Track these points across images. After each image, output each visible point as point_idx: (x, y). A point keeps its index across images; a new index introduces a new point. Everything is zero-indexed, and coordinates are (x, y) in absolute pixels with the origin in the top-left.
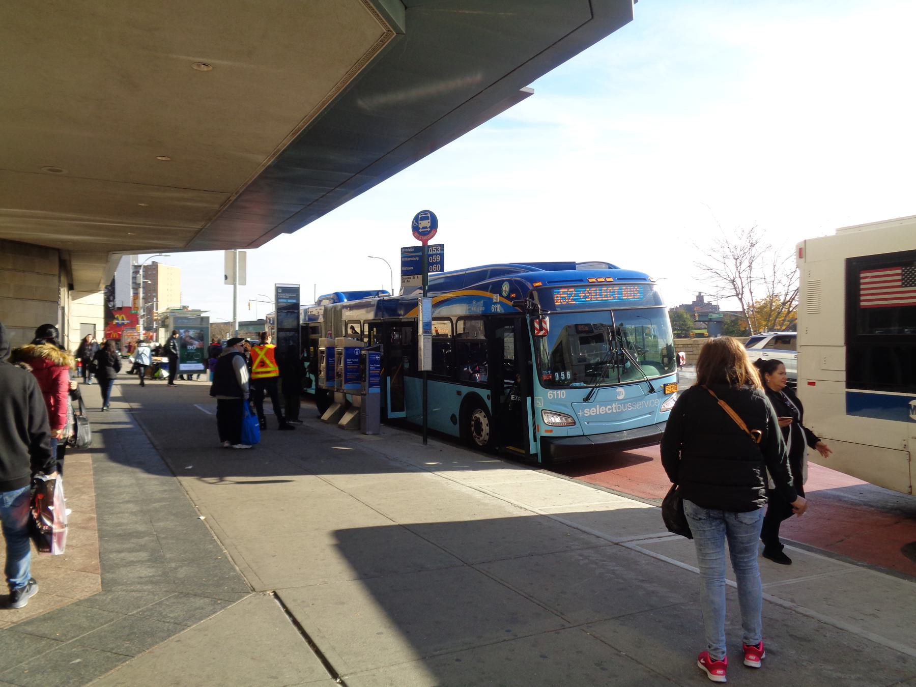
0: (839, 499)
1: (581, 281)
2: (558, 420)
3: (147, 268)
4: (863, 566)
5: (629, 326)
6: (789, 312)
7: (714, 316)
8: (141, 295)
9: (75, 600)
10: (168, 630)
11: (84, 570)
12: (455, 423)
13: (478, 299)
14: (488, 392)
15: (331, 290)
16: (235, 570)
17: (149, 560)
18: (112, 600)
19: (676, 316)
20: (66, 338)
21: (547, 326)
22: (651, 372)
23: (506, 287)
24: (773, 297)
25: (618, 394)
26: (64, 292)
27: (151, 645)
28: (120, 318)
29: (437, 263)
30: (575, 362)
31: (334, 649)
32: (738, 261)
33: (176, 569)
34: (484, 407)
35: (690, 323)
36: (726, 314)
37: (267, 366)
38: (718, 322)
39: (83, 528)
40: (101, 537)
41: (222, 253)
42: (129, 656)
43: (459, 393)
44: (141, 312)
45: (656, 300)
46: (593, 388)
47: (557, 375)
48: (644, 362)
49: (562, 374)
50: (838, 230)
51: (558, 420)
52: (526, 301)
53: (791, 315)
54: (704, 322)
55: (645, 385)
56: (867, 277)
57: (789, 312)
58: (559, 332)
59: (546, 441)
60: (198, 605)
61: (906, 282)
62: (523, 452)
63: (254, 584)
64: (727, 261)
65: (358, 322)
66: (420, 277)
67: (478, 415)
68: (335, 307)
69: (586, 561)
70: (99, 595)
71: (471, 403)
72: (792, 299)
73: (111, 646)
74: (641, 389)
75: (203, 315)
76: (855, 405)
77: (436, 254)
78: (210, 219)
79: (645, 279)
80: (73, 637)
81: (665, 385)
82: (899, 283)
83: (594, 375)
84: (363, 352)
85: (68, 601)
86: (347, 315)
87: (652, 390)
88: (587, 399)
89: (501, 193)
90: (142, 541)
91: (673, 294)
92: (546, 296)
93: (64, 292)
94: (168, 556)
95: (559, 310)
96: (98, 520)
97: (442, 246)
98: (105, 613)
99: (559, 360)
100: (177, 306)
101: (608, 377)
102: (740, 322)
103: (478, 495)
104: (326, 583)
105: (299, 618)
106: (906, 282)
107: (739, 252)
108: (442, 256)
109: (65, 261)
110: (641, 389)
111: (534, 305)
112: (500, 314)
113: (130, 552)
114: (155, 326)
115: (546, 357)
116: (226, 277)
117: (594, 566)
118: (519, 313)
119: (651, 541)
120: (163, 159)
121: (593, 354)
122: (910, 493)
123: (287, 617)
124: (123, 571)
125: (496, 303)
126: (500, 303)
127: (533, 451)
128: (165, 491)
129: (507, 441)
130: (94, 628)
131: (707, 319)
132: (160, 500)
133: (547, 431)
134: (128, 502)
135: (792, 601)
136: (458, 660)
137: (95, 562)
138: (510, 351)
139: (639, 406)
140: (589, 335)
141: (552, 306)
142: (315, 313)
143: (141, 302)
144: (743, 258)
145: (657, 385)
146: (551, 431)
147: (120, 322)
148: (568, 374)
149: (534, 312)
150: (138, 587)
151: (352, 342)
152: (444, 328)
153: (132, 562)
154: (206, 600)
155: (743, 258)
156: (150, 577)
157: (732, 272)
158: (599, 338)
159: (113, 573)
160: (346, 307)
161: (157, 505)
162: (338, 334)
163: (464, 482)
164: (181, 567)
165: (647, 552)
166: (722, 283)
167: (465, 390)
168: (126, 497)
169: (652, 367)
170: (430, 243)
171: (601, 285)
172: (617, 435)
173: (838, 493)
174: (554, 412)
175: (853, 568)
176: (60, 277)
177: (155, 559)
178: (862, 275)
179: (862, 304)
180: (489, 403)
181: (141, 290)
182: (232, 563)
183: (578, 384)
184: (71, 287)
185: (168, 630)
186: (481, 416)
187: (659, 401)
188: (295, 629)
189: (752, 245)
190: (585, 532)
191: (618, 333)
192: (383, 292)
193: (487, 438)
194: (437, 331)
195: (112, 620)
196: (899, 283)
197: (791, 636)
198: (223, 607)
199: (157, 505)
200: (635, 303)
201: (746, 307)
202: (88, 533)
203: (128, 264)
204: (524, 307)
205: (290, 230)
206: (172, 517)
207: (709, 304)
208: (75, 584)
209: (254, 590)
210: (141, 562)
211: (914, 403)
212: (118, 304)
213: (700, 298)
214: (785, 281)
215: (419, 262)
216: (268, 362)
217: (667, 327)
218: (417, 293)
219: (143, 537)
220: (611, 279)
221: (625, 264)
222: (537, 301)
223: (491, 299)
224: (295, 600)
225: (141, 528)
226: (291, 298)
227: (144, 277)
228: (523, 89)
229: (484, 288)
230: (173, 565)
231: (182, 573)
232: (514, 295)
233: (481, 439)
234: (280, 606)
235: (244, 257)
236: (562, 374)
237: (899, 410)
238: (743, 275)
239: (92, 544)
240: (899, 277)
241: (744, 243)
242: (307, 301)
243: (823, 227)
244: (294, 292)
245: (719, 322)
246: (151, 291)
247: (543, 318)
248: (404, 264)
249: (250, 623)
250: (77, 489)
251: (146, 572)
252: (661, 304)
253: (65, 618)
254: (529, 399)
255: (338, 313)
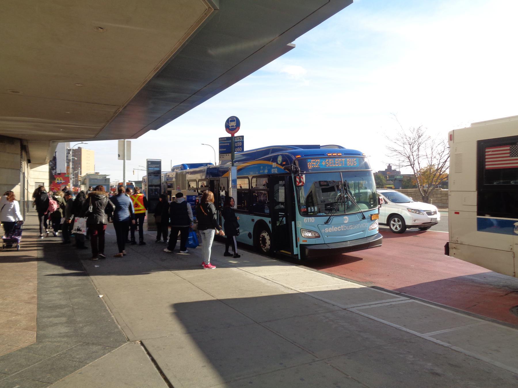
0: (473, 281)
1: (323, 155)
2: (310, 235)
3: (75, 151)
4: (489, 321)
5: (351, 182)
6: (440, 174)
7: (398, 177)
8: (71, 166)
9: (19, 348)
10: (75, 366)
11: (26, 329)
12: (250, 237)
13: (264, 166)
14: (270, 219)
15: (180, 163)
16: (118, 328)
17: (66, 323)
18: (42, 347)
19: (377, 176)
20: (26, 191)
21: (304, 180)
22: (363, 207)
23: (280, 159)
24: (431, 166)
25: (345, 220)
26: (24, 164)
27: (64, 376)
28: (59, 180)
29: (239, 147)
30: (319, 202)
31: (175, 377)
32: (411, 146)
33: (82, 327)
34: (267, 229)
35: (384, 181)
36: (404, 176)
37: (139, 206)
38: (400, 180)
39: (29, 303)
40: (38, 309)
41: (115, 143)
42: (50, 383)
43: (253, 220)
44: (71, 176)
45: (366, 166)
46: (330, 216)
47: (309, 208)
48: (359, 202)
49: (312, 208)
50: (472, 124)
51: (310, 235)
52: (291, 166)
53: (441, 177)
54: (392, 180)
55: (360, 215)
56: (489, 152)
57: (440, 174)
58: (311, 186)
59: (303, 247)
60: (94, 350)
61: (512, 154)
62: (290, 253)
63: (129, 336)
64: (405, 146)
65: (195, 180)
66: (230, 154)
67: (264, 234)
68: (182, 173)
69: (327, 320)
70: (34, 344)
71: (260, 227)
72: (442, 167)
73: (39, 377)
74: (358, 217)
75: (107, 177)
76: (482, 225)
77: (239, 142)
78: (108, 121)
79: (359, 154)
80: (16, 372)
81: (371, 215)
82: (508, 155)
83: (330, 209)
84: (197, 198)
85: (15, 348)
86: (189, 177)
87: (364, 218)
88: (326, 223)
89: (278, 105)
90: (63, 311)
91: (376, 165)
92: (303, 163)
93: (24, 164)
94: (78, 319)
95: (310, 171)
96: (38, 298)
97: (243, 137)
98: (37, 356)
99: (310, 201)
100: (92, 172)
101: (338, 210)
102: (412, 180)
103: (264, 281)
104: (172, 335)
105: (155, 358)
106: (512, 154)
107: (412, 141)
108: (243, 142)
109: (25, 146)
110: (358, 217)
111: (296, 168)
112: (277, 174)
113: (55, 317)
114: (79, 184)
115: (303, 201)
116: (119, 156)
117: (332, 323)
118: (288, 173)
119: (364, 307)
120: (79, 85)
121: (331, 197)
122: (514, 276)
123: (148, 356)
124: (50, 329)
125: (274, 168)
126: (277, 167)
127: (295, 252)
128: (80, 280)
129: (281, 249)
130: (29, 366)
131: (393, 179)
132: (75, 286)
133: (304, 241)
134: (57, 287)
135: (449, 343)
136: (251, 383)
137: (34, 324)
138: (281, 196)
139: (357, 227)
140: (328, 188)
141: (307, 170)
142: (170, 176)
143: (71, 170)
144: (415, 143)
145: (367, 215)
146: (306, 241)
147: (59, 181)
148: (316, 208)
149: (296, 172)
150: (59, 339)
151: (192, 193)
152: (243, 184)
153: (56, 323)
154: (100, 347)
155: (415, 143)
156: (67, 333)
157: (408, 152)
158: (332, 189)
159: (44, 330)
160: (188, 173)
161: (74, 289)
162: (184, 188)
163: (255, 274)
164: (85, 326)
165: (363, 314)
166: (402, 158)
167: (257, 218)
168: (56, 284)
169: (364, 205)
170: (236, 135)
171: (334, 157)
172: (344, 243)
173: (471, 278)
174: (307, 230)
175: (483, 322)
176: (21, 155)
177: (71, 321)
178: (487, 150)
179: (487, 167)
180: (270, 226)
181: (71, 163)
182: (116, 323)
183: (321, 214)
184: (29, 161)
185: (75, 366)
186: (265, 235)
187: (368, 224)
188: (153, 364)
189: (419, 137)
190: (326, 302)
191: (345, 185)
192: (210, 164)
193: (269, 247)
194: (241, 187)
195: (41, 360)
196: (508, 155)
197: (449, 364)
198: (110, 351)
199: (74, 289)
200: (355, 168)
201: (416, 172)
202: (31, 306)
203: (64, 148)
204: (290, 170)
205: (156, 128)
206: (83, 296)
207: (395, 170)
208: (20, 338)
209: (129, 340)
210: (61, 324)
211: (516, 224)
212: (58, 171)
213: (390, 167)
214: (438, 157)
215: (230, 146)
216: (140, 204)
217: (372, 181)
218: (229, 164)
219: (65, 308)
220: (340, 154)
221: (348, 146)
222: (298, 166)
223: (272, 166)
224: (153, 346)
225: (63, 302)
226: (156, 167)
227: (73, 156)
228: (289, 44)
229: (268, 159)
230: (81, 325)
231: (86, 330)
232: (284, 163)
233: (266, 248)
234: (144, 350)
235: (129, 143)
236: (312, 208)
237: (507, 228)
238: (415, 154)
239: (33, 313)
240: (509, 151)
241: (415, 135)
242: (166, 168)
243: (464, 121)
244: (158, 164)
245: (401, 181)
246: (77, 164)
247: (301, 175)
248: (221, 147)
249: (126, 359)
250: (27, 279)
251: (63, 329)
252: (369, 168)
253: (12, 359)
254: (293, 223)
255: (184, 176)
